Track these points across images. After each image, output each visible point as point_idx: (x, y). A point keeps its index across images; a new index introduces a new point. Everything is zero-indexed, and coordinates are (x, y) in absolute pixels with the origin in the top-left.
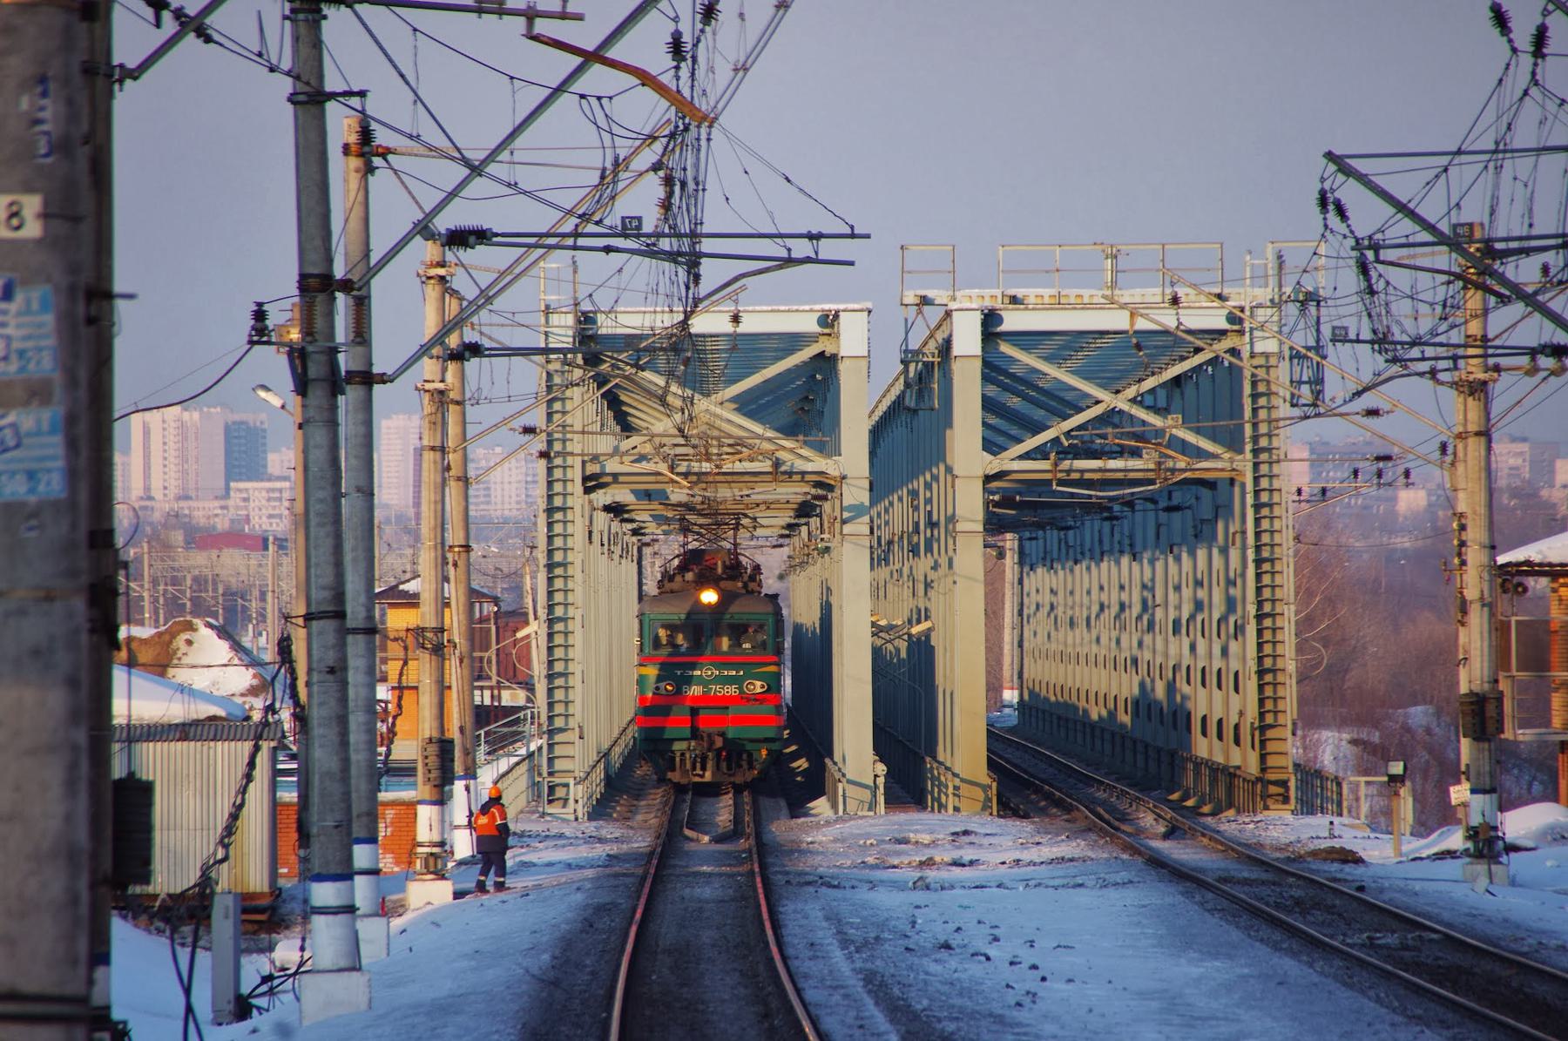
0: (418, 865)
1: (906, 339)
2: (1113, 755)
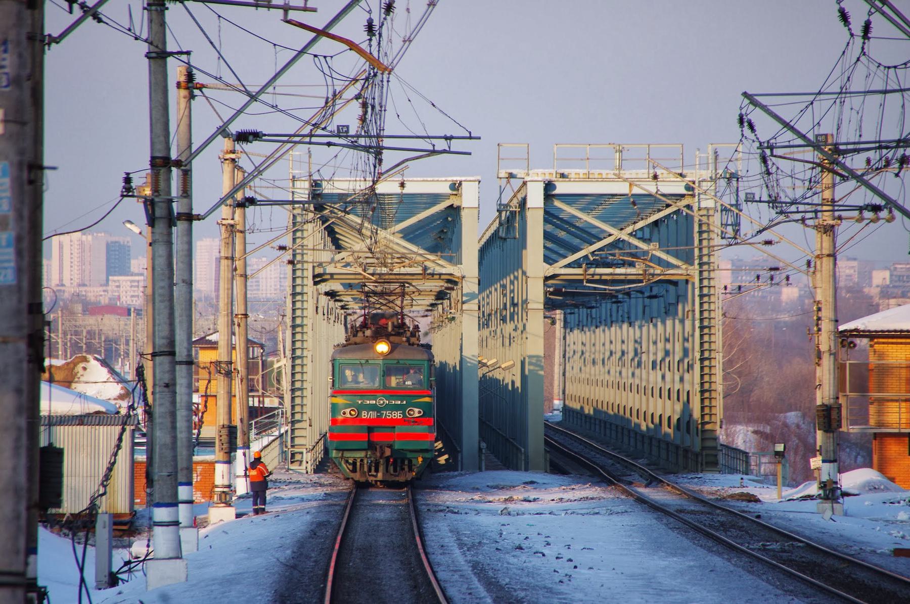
0: (216, 498)
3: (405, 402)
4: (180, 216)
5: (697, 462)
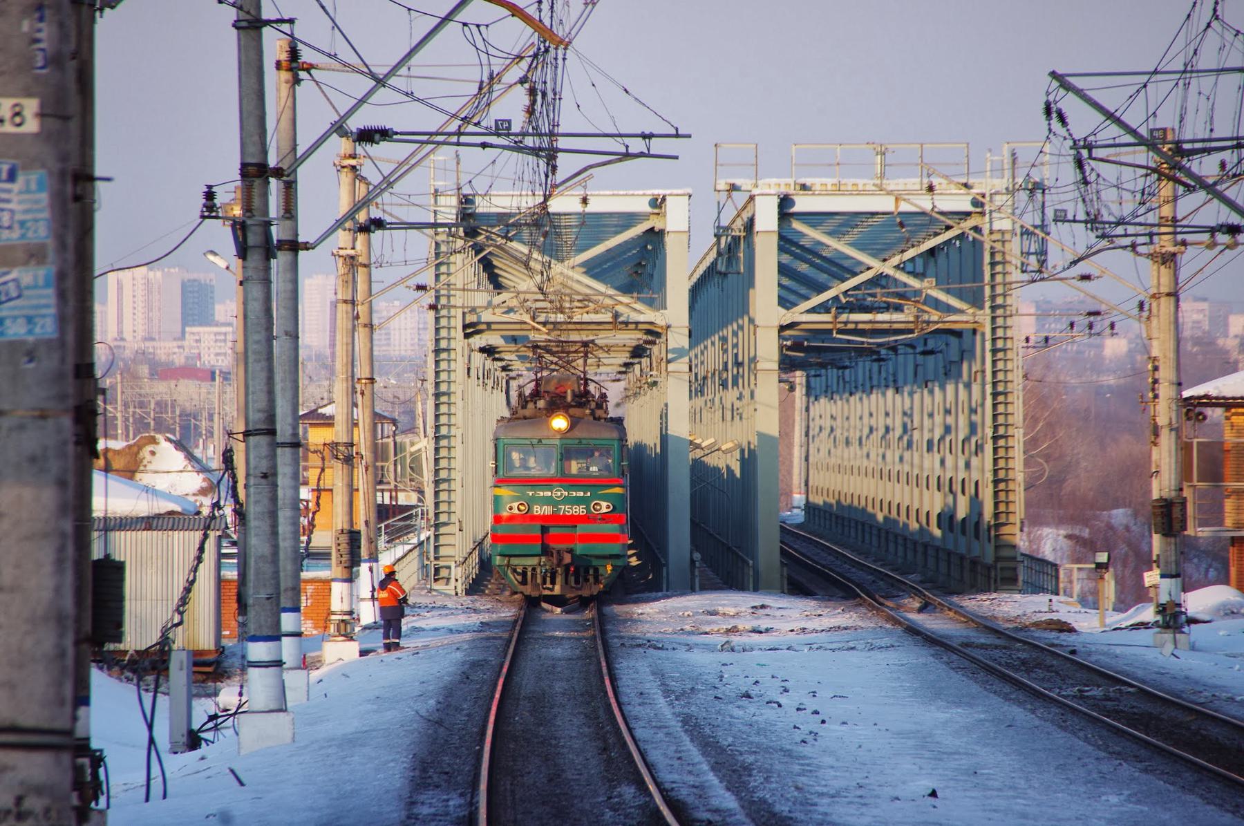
0: (332, 629)
3: (589, 494)
4: (281, 244)
5: (989, 578)
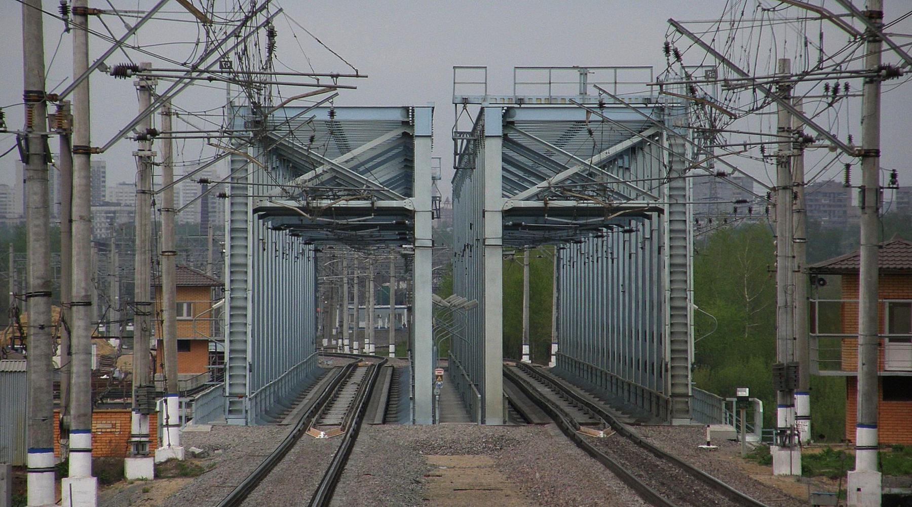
1: (456, 125)
2: (601, 385)
5: (667, 409)
